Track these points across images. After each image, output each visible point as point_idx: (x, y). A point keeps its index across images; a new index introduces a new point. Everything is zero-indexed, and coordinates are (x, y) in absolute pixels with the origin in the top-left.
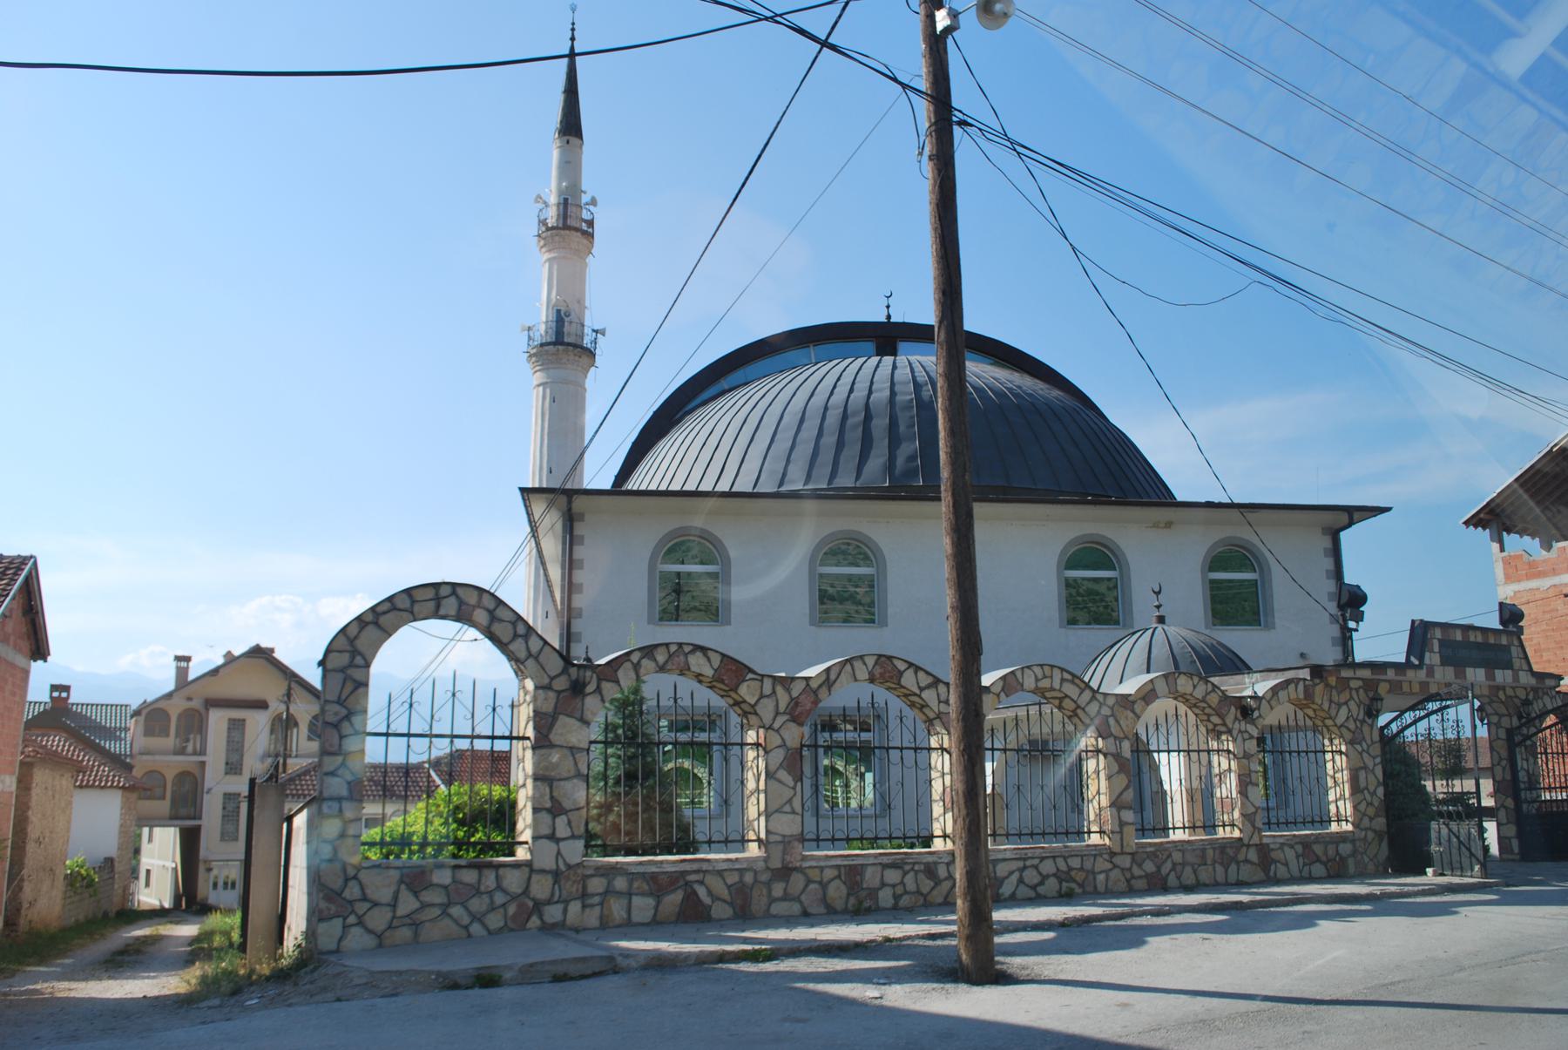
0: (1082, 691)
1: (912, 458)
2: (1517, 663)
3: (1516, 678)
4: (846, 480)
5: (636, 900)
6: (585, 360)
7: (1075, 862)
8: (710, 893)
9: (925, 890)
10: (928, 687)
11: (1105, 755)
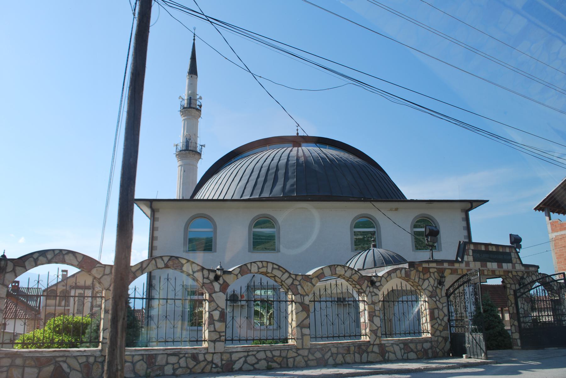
0: (284, 273)
1: (292, 185)
2: (514, 260)
3: (514, 267)
4: (266, 194)
5: (27, 370)
6: (197, 156)
7: (277, 353)
8: (69, 366)
9: (191, 367)
10: (198, 271)
11: (295, 303)
